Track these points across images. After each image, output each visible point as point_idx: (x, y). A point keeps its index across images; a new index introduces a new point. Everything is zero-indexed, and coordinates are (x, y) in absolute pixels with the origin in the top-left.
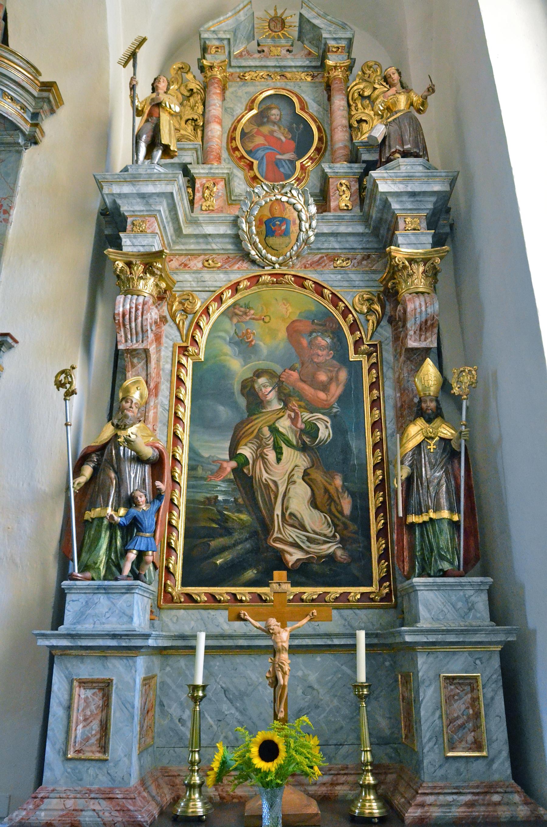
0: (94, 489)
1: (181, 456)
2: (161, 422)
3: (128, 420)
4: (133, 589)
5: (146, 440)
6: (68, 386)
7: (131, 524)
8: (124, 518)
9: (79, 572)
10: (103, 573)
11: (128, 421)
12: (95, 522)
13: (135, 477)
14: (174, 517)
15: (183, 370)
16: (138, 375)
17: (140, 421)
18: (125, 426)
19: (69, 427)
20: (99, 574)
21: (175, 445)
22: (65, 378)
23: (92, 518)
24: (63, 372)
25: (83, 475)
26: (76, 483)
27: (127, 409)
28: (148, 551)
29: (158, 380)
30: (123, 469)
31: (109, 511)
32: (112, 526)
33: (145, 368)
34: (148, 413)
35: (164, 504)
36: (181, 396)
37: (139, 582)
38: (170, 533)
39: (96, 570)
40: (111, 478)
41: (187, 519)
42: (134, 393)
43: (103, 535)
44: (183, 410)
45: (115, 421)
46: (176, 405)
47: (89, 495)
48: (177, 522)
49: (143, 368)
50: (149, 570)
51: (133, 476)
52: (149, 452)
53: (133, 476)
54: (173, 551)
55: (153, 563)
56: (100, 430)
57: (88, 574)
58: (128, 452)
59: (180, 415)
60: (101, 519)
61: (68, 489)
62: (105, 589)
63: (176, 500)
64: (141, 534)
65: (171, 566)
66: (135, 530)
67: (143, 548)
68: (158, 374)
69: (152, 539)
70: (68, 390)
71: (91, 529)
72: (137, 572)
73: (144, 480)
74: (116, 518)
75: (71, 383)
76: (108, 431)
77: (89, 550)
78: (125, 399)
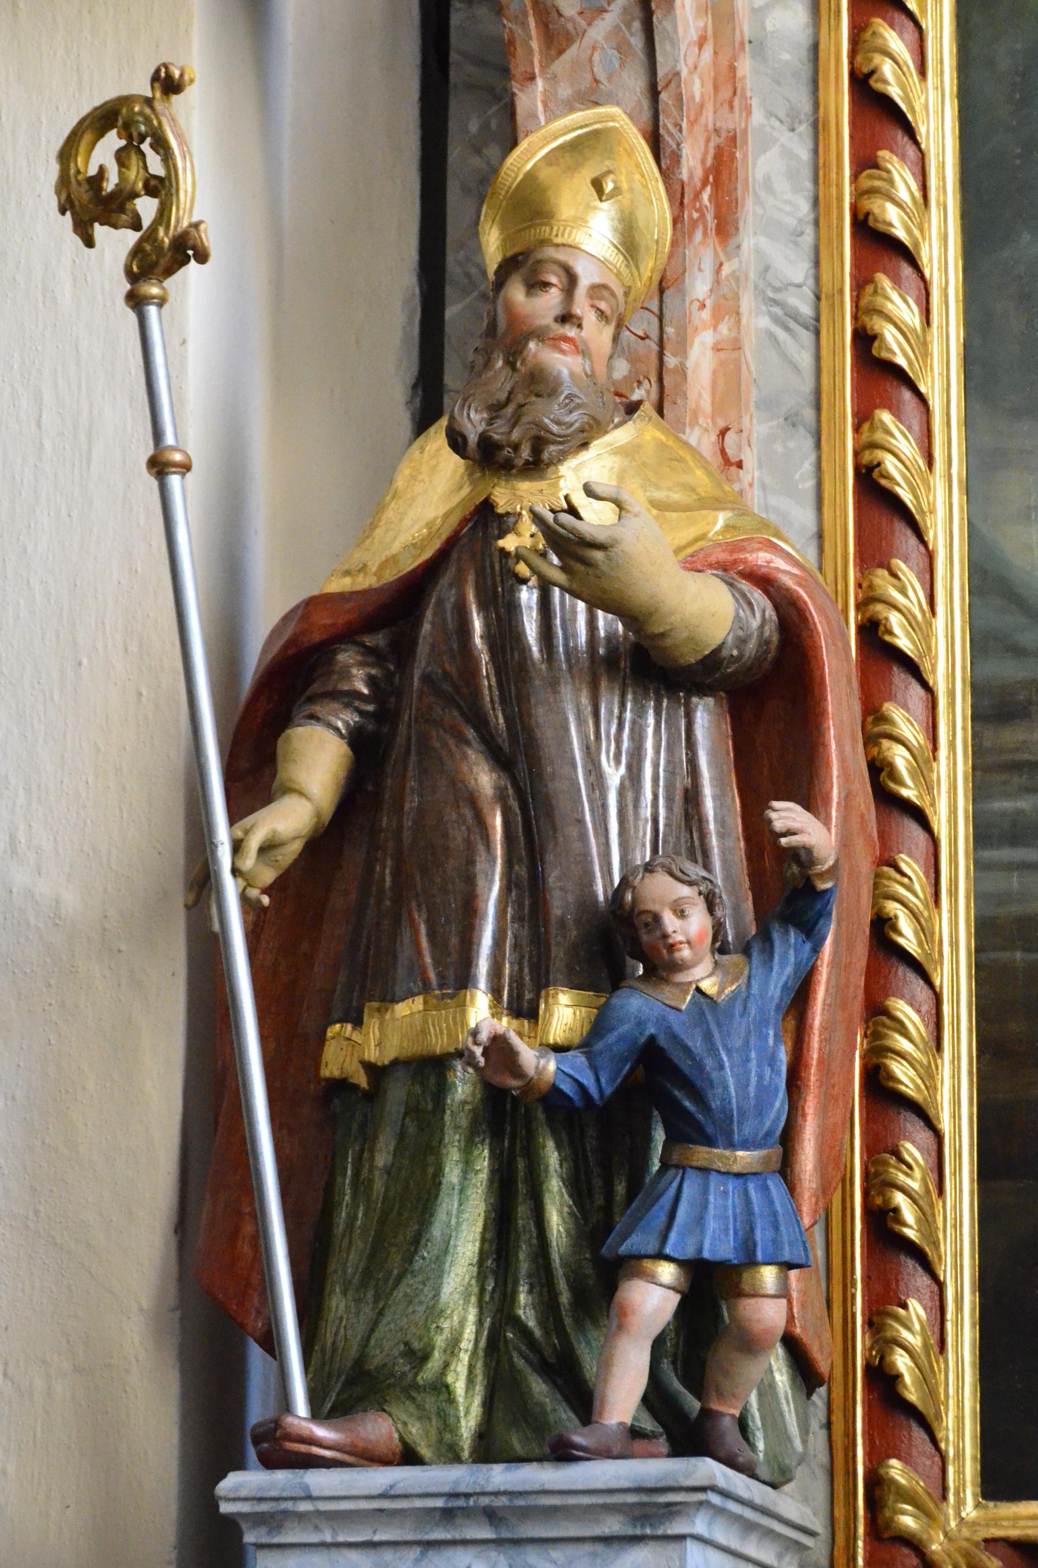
0: (368, 880)
1: (922, 630)
2: (767, 405)
3: (556, 409)
4: (672, 1511)
5: (686, 535)
6: (146, 207)
7: (626, 1091)
8: (578, 1058)
9: (316, 1414)
10: (469, 1419)
11: (551, 415)
12: (397, 1093)
13: (630, 780)
14: (902, 1044)
15: (895, 41)
16: (590, 98)
17: (632, 409)
18: (539, 444)
19: (174, 480)
20: (447, 1424)
21: (873, 554)
22: (121, 157)
23: (369, 1067)
24: (106, 118)
25: (288, 789)
26: (254, 843)
27: (540, 335)
28: (752, 1263)
29: (730, 121)
30: (546, 735)
31: (480, 1011)
32: (510, 1111)
33: (637, 42)
34: (682, 349)
35: (836, 956)
36: (895, 220)
37: (707, 1469)
38: (881, 1149)
39: (430, 1402)
40: (472, 800)
41: (993, 1051)
42: (580, 221)
43: (452, 1174)
44: (907, 312)
45: (474, 423)
46: (862, 282)
47: (344, 919)
48: (929, 1075)
49: (622, 48)
50: (767, 1391)
51: (614, 775)
52: (709, 613)
53: (614, 775)
54: (910, 1265)
55: (792, 1344)
56: (375, 492)
57: (378, 1428)
58: (569, 622)
59: (895, 347)
60: (430, 1069)
61: (202, 883)
62: (491, 1515)
63: (905, 924)
64: (702, 1154)
65: (902, 1362)
66: (659, 1136)
67: (718, 1245)
68: (727, 82)
69: (776, 1186)
70: (150, 236)
71: (368, 1139)
72: (694, 1405)
73: (692, 797)
74: (528, 1056)
75: (160, 187)
76: (432, 488)
77: (367, 1274)
78: (523, 264)
